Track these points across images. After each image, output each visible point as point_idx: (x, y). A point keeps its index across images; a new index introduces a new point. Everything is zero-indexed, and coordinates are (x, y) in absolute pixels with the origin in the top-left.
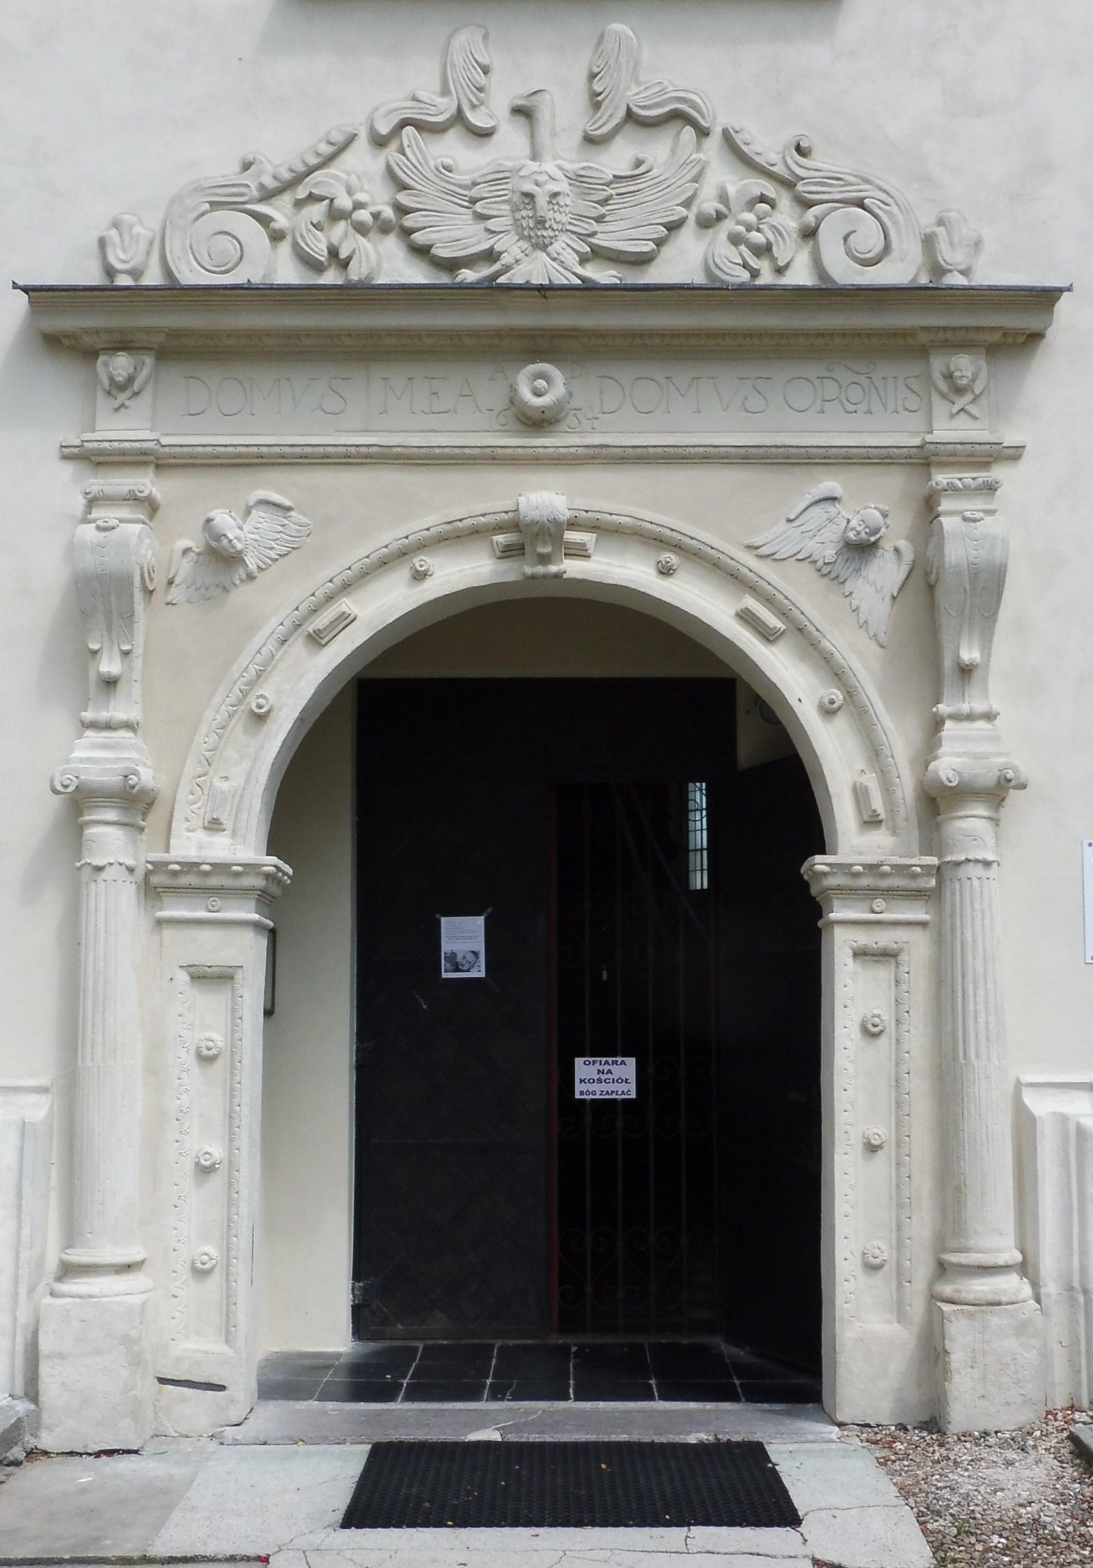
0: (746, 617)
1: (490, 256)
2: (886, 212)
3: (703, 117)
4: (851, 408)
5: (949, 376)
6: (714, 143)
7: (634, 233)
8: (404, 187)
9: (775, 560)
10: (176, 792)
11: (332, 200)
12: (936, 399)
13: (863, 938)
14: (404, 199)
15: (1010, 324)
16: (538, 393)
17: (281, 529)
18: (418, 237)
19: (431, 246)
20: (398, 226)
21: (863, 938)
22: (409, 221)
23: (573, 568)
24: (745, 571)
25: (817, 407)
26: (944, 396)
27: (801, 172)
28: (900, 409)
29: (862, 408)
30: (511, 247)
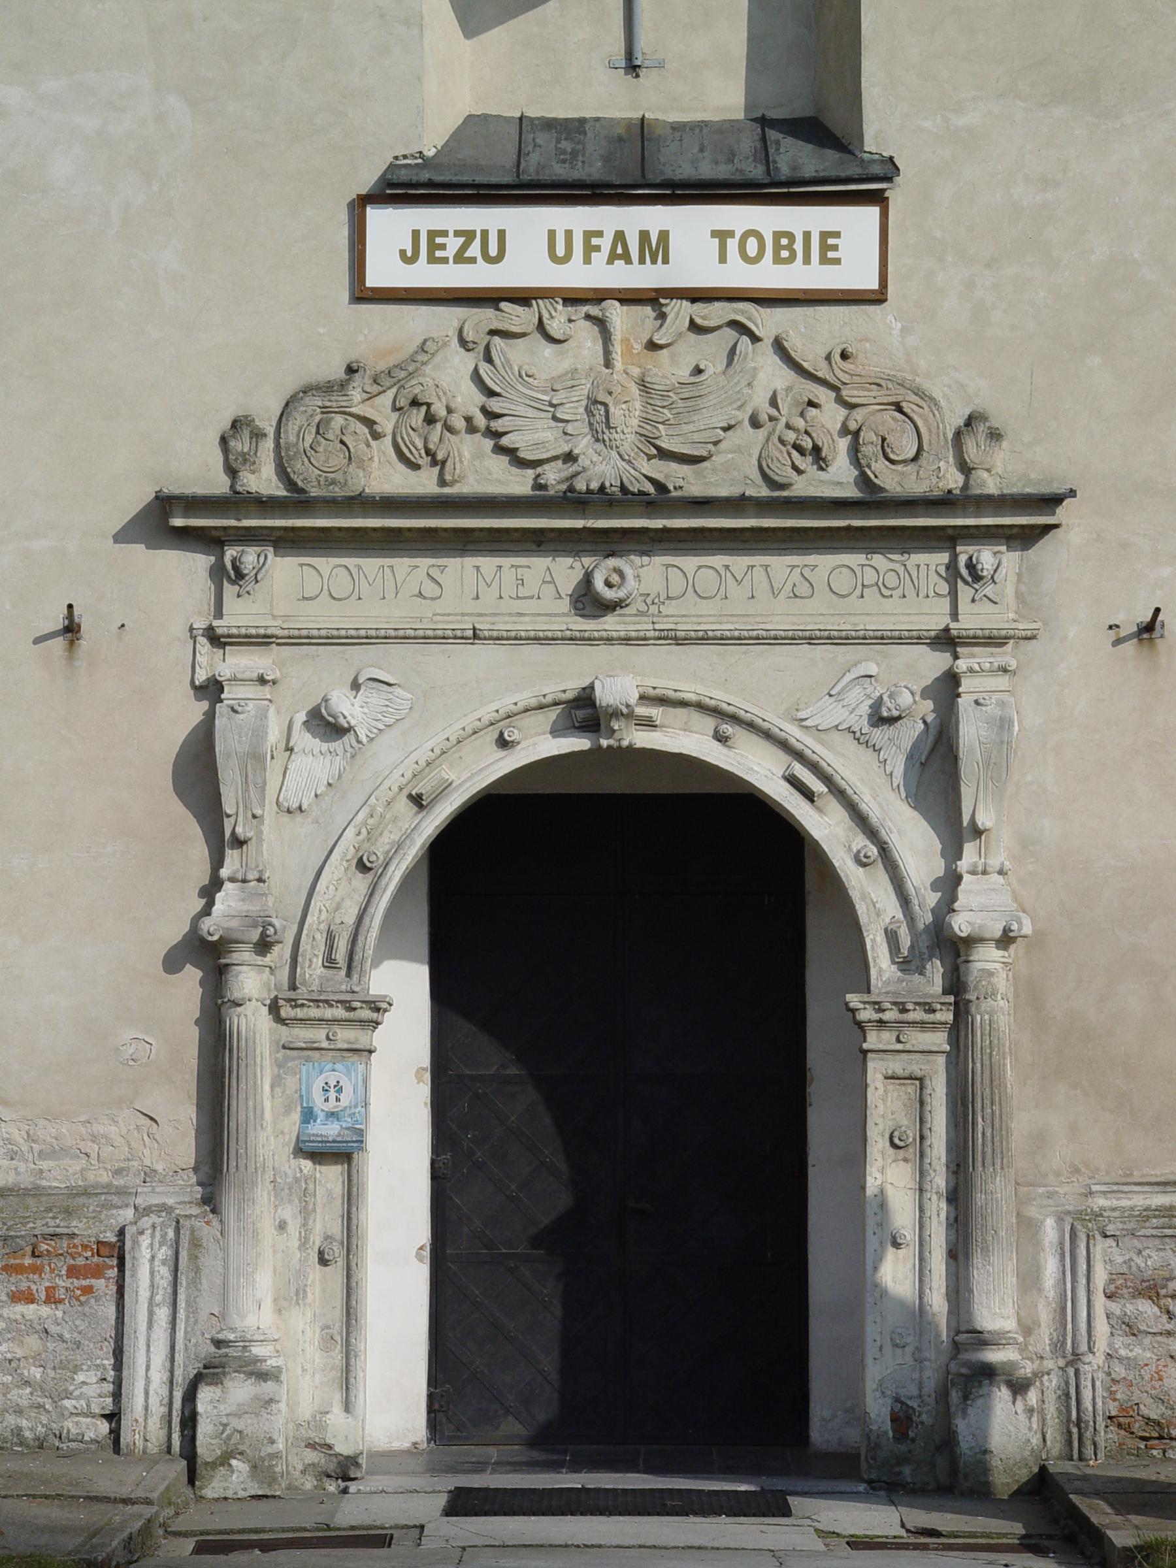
0: (794, 782)
1: (570, 457)
2: (921, 416)
3: (757, 326)
4: (886, 592)
5: (971, 566)
6: (766, 346)
7: (696, 437)
8: (491, 393)
9: (807, 727)
10: (385, 1474)
11: (429, 405)
12: (960, 584)
13: (896, 1065)
14: (495, 405)
15: (1029, 518)
16: (609, 584)
17: (380, 717)
18: (505, 441)
19: (517, 449)
20: (491, 429)
21: (896, 1065)
22: (497, 425)
23: (642, 739)
24: (794, 741)
25: (858, 592)
26: (966, 583)
27: (845, 378)
28: (932, 594)
29: (897, 593)
30: (583, 445)
